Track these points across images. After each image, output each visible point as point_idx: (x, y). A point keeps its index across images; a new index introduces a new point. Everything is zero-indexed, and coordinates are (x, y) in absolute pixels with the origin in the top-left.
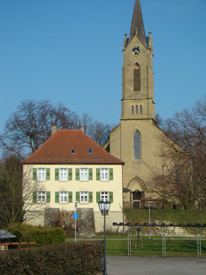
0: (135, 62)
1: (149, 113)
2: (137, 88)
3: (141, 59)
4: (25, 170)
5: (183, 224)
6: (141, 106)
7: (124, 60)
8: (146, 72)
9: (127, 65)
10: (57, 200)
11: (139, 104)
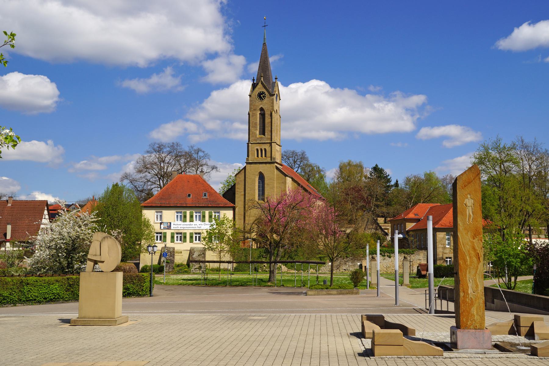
2: (263, 132)
6: (265, 150)
8: (269, 117)
10: (172, 241)
11: (263, 148)
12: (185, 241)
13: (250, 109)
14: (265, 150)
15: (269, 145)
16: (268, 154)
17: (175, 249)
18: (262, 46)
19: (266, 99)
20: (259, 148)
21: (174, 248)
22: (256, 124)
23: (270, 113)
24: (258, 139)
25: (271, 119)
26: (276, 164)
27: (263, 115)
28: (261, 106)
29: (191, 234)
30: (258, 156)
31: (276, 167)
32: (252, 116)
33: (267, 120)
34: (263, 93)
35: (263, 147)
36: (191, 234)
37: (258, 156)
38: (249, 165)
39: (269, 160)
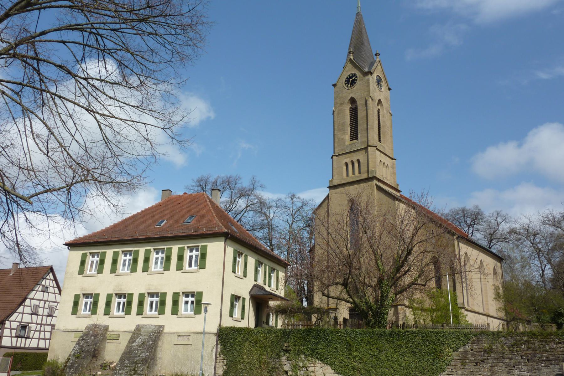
0: (349, 98)
1: (370, 169)
2: (354, 136)
3: (379, 107)
4: (412, 258)
5: (519, 221)
6: (359, 161)
7: (335, 98)
8: (364, 108)
9: (338, 105)
12: (128, 312)
13: (336, 104)
14: (359, 161)
15: (363, 152)
16: (364, 168)
17: (110, 329)
18: (355, 17)
19: (358, 83)
20: (348, 160)
21: (106, 328)
22: (344, 124)
23: (364, 102)
24: (347, 146)
25: (367, 110)
26: (375, 182)
27: (354, 112)
28: (351, 95)
29: (176, 296)
30: (348, 175)
31: (378, 187)
32: (338, 114)
33: (361, 114)
34: (354, 75)
35: (355, 157)
36: (142, 296)
37: (348, 175)
38: (334, 191)
39: (365, 176)
